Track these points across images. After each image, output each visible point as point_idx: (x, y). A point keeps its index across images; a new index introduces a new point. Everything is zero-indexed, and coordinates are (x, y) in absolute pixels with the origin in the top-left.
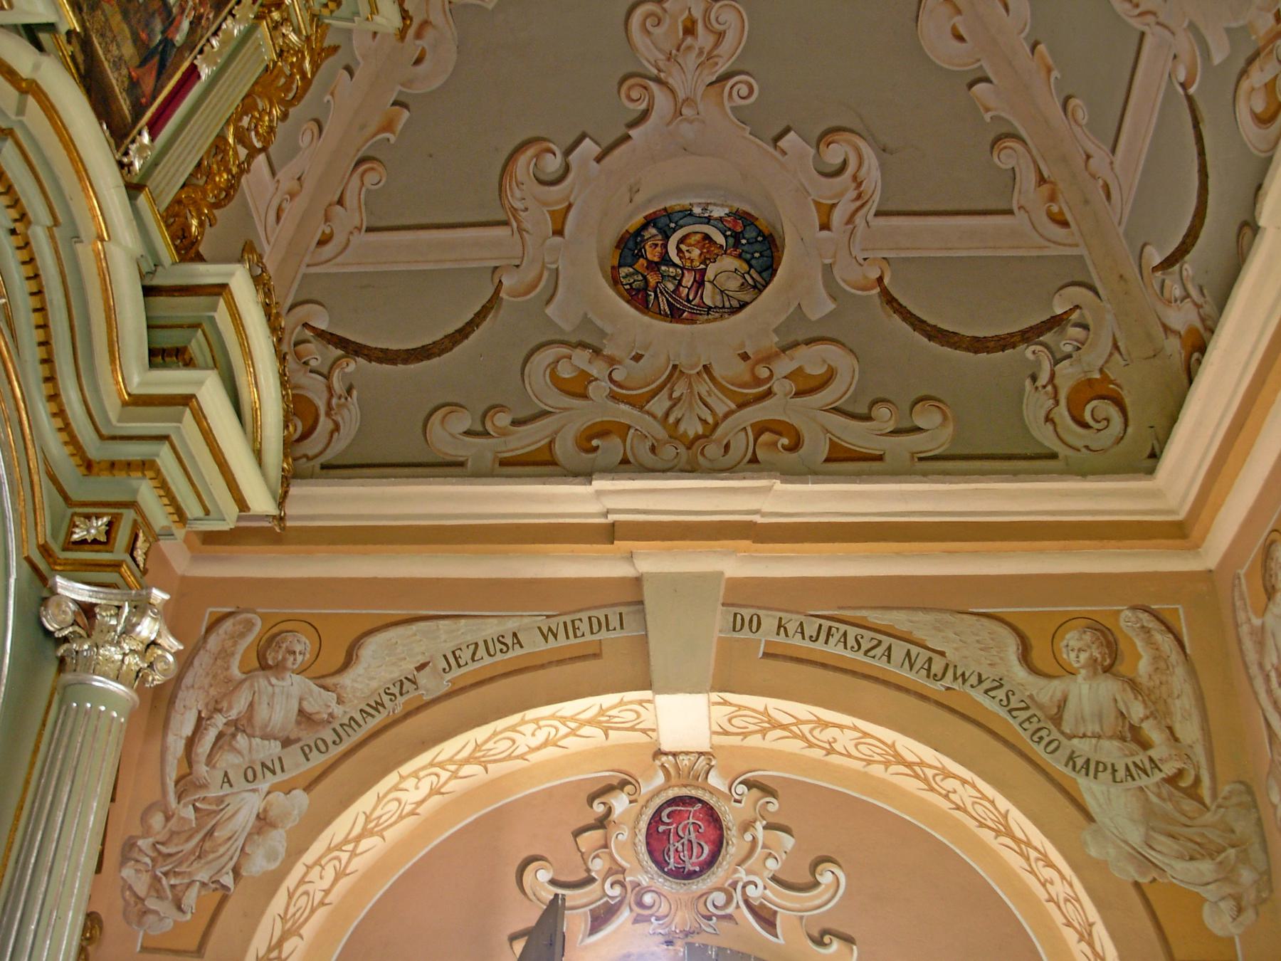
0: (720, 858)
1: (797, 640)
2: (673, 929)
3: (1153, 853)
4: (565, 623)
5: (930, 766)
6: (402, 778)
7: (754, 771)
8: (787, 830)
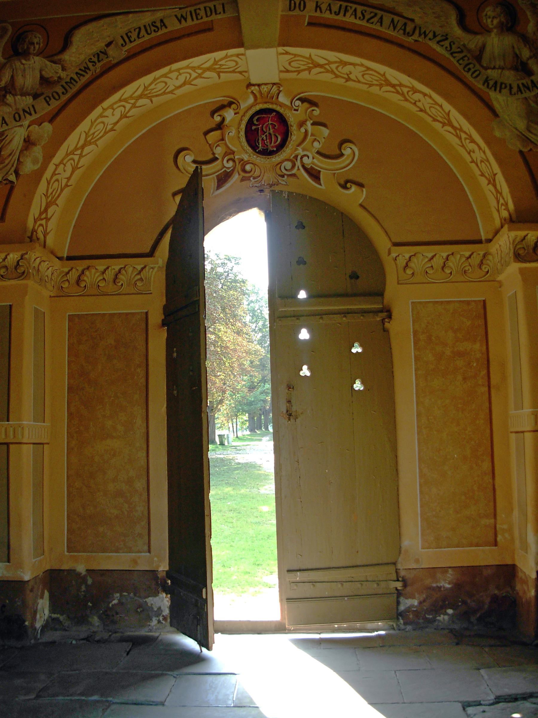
0: (287, 143)
1: (327, 15)
2: (263, 183)
3: (530, 134)
4: (191, 12)
5: (406, 87)
6: (104, 110)
7: (305, 92)
8: (324, 125)
